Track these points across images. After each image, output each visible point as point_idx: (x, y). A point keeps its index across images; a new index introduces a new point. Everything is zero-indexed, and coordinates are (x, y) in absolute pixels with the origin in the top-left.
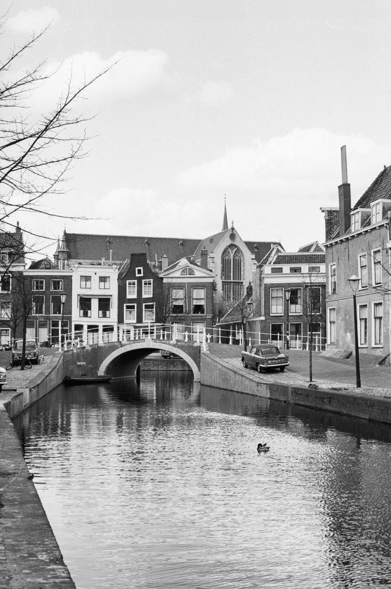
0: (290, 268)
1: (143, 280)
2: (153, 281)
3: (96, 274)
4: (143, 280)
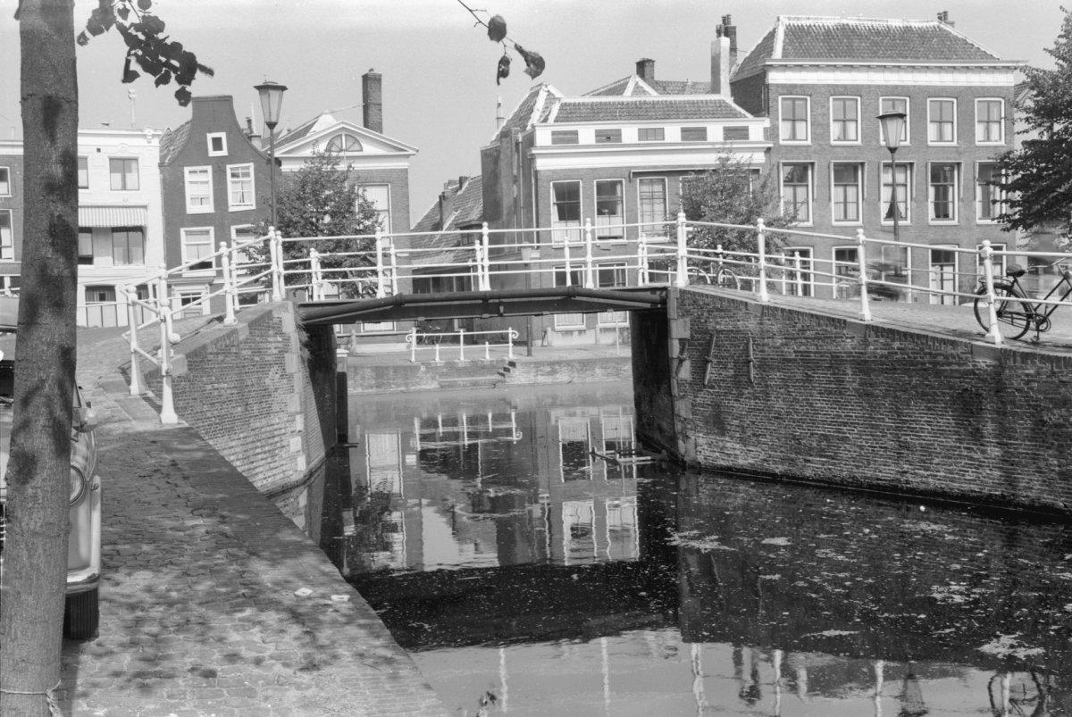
0: (682, 128)
1: (228, 167)
2: (255, 169)
3: (99, 150)
4: (228, 167)
